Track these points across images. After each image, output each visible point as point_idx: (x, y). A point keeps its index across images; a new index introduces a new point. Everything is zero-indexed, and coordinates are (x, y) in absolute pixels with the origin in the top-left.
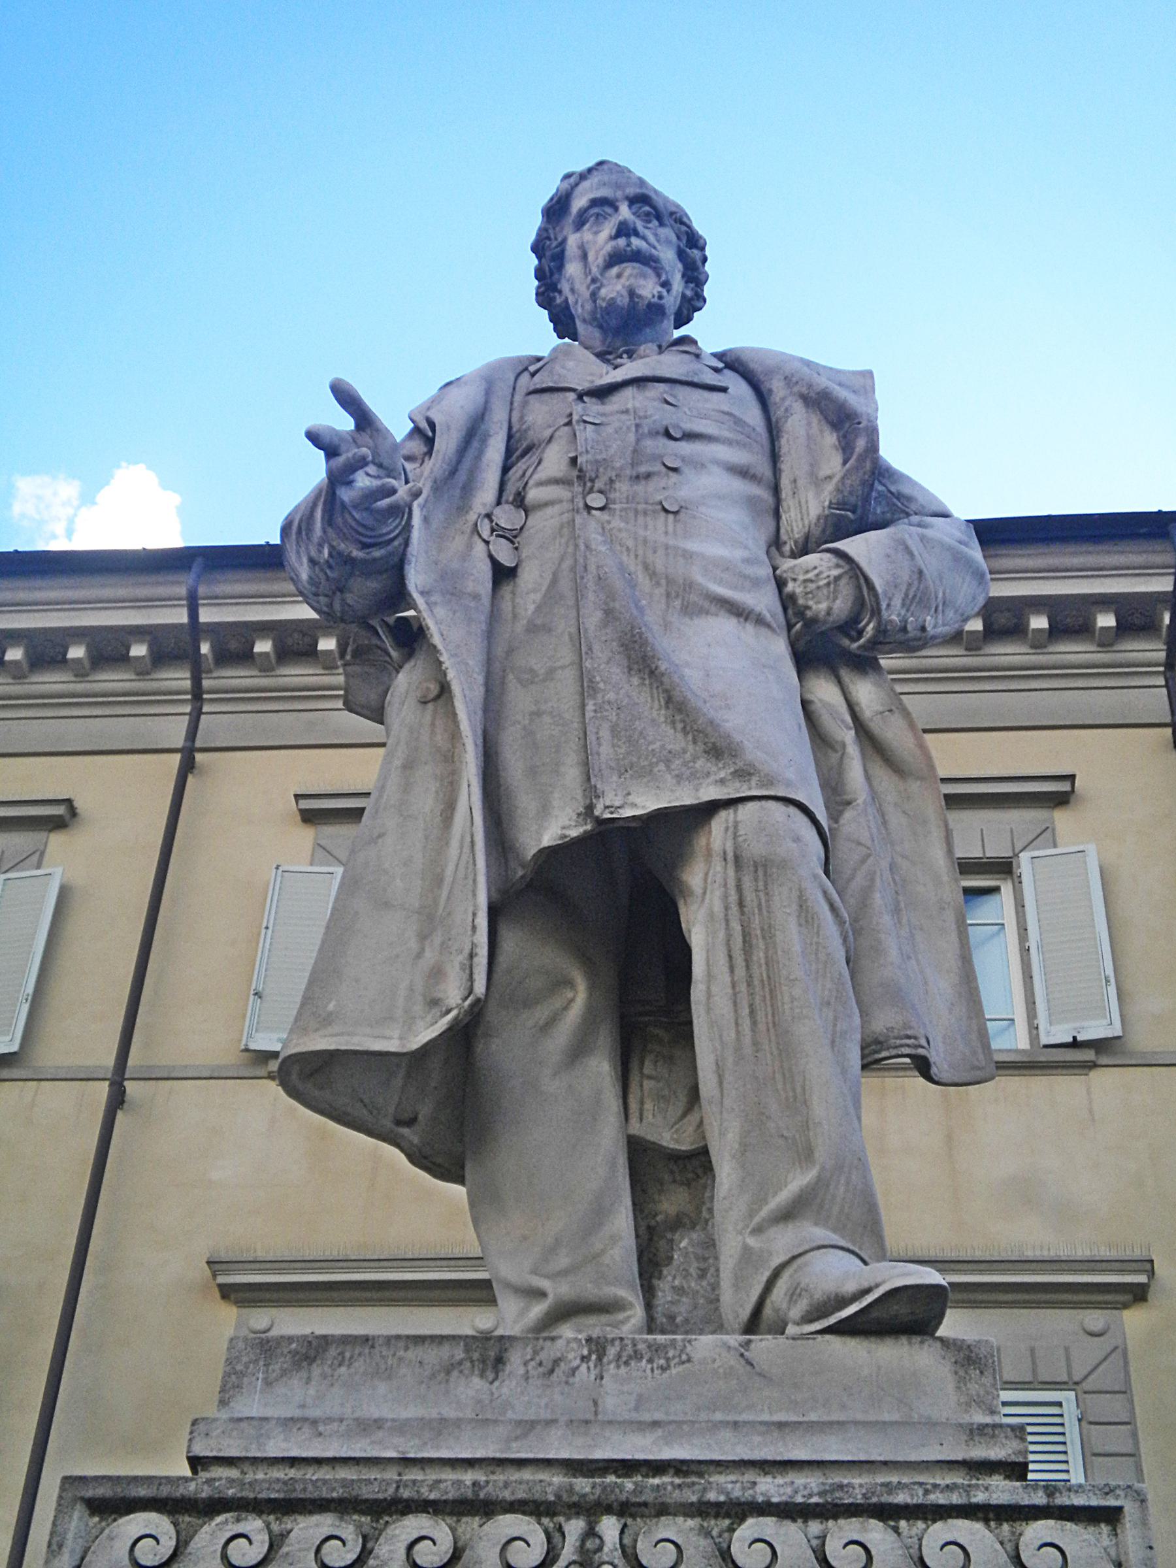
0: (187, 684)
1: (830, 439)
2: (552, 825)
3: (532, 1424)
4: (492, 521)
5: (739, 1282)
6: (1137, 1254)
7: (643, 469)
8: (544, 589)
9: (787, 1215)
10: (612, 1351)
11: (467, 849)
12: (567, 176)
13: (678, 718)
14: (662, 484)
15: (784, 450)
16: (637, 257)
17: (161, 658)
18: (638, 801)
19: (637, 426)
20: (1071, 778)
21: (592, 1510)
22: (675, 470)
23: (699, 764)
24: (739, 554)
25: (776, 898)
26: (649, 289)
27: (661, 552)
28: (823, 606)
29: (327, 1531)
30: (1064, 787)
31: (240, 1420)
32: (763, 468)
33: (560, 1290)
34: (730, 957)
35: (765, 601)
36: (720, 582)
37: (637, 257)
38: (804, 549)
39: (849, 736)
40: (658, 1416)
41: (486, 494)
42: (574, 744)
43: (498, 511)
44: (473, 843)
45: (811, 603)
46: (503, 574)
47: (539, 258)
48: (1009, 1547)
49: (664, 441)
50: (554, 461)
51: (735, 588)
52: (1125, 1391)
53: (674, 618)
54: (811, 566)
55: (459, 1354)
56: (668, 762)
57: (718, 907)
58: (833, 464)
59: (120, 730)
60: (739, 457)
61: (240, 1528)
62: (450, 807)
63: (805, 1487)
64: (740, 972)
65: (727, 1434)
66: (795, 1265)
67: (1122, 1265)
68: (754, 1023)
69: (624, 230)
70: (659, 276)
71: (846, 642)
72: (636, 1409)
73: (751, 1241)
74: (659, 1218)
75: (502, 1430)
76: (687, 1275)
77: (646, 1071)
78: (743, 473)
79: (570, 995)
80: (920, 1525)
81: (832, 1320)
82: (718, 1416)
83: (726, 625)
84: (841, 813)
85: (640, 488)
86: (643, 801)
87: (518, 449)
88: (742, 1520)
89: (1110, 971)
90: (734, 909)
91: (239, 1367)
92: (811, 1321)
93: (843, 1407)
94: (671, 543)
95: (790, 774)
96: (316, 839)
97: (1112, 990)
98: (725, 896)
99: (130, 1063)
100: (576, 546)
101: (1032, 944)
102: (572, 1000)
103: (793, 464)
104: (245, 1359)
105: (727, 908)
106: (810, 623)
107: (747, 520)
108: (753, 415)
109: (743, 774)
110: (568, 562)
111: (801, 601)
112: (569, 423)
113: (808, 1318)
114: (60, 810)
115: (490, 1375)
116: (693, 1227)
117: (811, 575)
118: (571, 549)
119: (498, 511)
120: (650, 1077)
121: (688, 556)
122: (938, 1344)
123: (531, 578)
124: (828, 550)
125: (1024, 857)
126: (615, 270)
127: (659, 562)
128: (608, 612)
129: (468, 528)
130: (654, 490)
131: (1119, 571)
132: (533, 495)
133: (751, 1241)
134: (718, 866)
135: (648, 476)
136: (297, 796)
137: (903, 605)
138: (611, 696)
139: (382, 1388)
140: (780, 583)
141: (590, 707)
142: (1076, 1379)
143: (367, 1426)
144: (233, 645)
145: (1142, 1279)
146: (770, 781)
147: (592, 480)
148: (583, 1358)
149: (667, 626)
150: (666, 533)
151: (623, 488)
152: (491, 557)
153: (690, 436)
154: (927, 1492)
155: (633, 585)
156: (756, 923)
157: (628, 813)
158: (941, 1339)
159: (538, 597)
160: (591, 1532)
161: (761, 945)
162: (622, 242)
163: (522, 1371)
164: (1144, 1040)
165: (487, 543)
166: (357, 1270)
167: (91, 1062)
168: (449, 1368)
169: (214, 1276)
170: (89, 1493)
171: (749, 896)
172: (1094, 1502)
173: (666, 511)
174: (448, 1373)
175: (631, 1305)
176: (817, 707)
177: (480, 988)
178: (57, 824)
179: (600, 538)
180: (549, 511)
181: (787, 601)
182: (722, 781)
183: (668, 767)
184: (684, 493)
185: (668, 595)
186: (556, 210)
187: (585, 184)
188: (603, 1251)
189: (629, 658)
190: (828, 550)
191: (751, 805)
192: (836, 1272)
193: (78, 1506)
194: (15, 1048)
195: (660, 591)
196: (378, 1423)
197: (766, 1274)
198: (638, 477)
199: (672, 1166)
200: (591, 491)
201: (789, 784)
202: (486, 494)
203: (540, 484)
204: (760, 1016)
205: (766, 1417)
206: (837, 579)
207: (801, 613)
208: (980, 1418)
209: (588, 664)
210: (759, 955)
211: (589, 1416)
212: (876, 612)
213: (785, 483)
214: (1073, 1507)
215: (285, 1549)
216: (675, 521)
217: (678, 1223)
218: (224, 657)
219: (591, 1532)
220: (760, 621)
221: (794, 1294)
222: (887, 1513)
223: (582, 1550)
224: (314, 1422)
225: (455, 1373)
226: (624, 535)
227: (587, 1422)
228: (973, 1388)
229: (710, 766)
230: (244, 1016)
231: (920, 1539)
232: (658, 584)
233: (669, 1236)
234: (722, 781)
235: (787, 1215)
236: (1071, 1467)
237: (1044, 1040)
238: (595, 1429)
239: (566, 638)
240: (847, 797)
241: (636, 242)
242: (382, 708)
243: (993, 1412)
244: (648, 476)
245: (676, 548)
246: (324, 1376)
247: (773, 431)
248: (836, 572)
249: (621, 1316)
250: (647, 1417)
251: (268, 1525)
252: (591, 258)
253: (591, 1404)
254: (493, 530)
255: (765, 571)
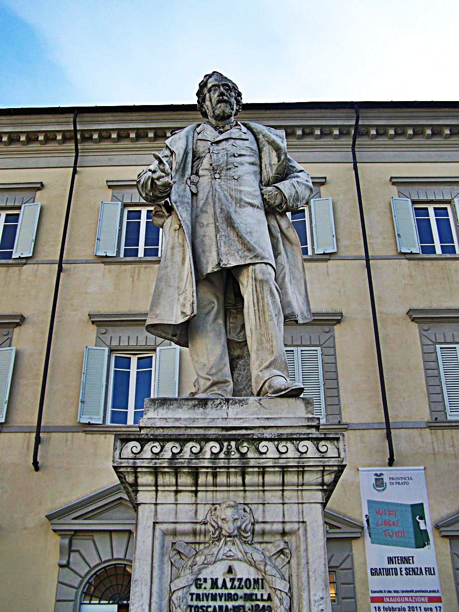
0: (74, 147)
1: (274, 154)
2: (210, 267)
3: (214, 419)
4: (190, 180)
5: (257, 383)
6: (339, 311)
7: (229, 167)
8: (204, 199)
9: (267, 368)
10: (231, 401)
11: (190, 274)
12: (206, 76)
13: (240, 240)
14: (233, 171)
15: (263, 157)
16: (225, 101)
17: (65, 140)
18: (231, 263)
19: (227, 154)
20: (325, 178)
21: (229, 440)
22: (237, 167)
23: (246, 253)
24: (253, 189)
25: (265, 290)
26: (228, 111)
27: (234, 191)
28: (273, 202)
29: (173, 445)
30: (324, 180)
31: (149, 418)
32: (258, 162)
33: (215, 379)
34: (254, 303)
35: (258, 201)
36: (248, 198)
37: (225, 101)
38: (268, 185)
39: (279, 235)
40: (241, 417)
41: (189, 172)
42: (214, 243)
43: (192, 177)
44: (191, 273)
45: (270, 201)
46: (194, 195)
47: (199, 97)
48: (316, 446)
49: (233, 158)
50: (206, 163)
51: (252, 199)
52: (334, 347)
53: (238, 209)
54: (270, 190)
55: (197, 403)
56: (238, 252)
57: (251, 290)
58: (275, 160)
59: (54, 161)
60: (252, 160)
61: (154, 445)
62: (184, 259)
63: (273, 433)
64: (256, 308)
65: (256, 420)
66: (270, 380)
67: (335, 314)
68: (260, 321)
69: (222, 94)
70: (231, 107)
71: (278, 210)
72: (237, 415)
73: (259, 373)
74: (234, 356)
75: (207, 420)
76: (240, 370)
77: (231, 321)
78: (252, 164)
79: (213, 305)
80: (298, 442)
81: (279, 394)
82: (254, 416)
83: (249, 209)
84: (277, 257)
85: (228, 172)
86: (233, 264)
87: (197, 157)
88: (261, 442)
89: (334, 234)
90: (255, 292)
91: (148, 406)
92: (274, 394)
93: (281, 414)
94: (236, 188)
95: (267, 256)
96: (113, 193)
97: (335, 239)
98: (253, 289)
99: (64, 259)
100: (213, 189)
101: (313, 225)
102: (214, 307)
103: (265, 160)
104: (149, 404)
105: (253, 291)
106: (269, 206)
107: (254, 179)
108: (255, 147)
109: (256, 257)
110: (211, 193)
111: (268, 200)
112: (209, 152)
113: (273, 393)
114: (39, 185)
115: (204, 407)
116: (242, 358)
117: (270, 193)
118: (211, 190)
119: (192, 177)
120: (231, 323)
121: (241, 191)
122: (301, 399)
123: (200, 195)
124: (274, 186)
125: (312, 200)
126: (219, 105)
127: (233, 193)
128: (222, 209)
129: (185, 182)
130: (231, 173)
131: (340, 118)
132: (201, 173)
133: (259, 373)
134: (250, 280)
135: (230, 169)
136: (107, 181)
137: (293, 201)
138: (223, 233)
139: (180, 410)
140: (262, 195)
141: (218, 236)
142: (321, 344)
143: (177, 420)
144: (87, 136)
145: (340, 318)
146: (263, 258)
147: (216, 170)
148: (224, 404)
149: (236, 212)
150: (235, 185)
151: (224, 172)
152: (191, 190)
153: (240, 155)
154: (300, 435)
155: (227, 200)
156: (260, 295)
157: (229, 266)
158: (301, 398)
159: (203, 201)
160: (229, 445)
161: (261, 301)
162: (221, 98)
163: (211, 406)
164: (343, 253)
165: (190, 187)
166: (129, 317)
167: (53, 259)
168: (195, 406)
169: (90, 318)
170: (121, 437)
171: (258, 289)
172: (334, 436)
173: (235, 179)
174: (195, 407)
175: (230, 382)
176: (271, 226)
177: (195, 312)
178: (38, 189)
179: (219, 187)
180: (205, 178)
181: (264, 200)
182: (251, 258)
183: (238, 254)
184: (239, 173)
185: (236, 203)
186: (203, 85)
187: (211, 80)
188: (223, 368)
189: (227, 223)
190: (274, 186)
191: (259, 265)
192: (280, 382)
193: (119, 440)
194: (31, 255)
195: (234, 202)
196: (180, 419)
197: (263, 381)
198: (227, 169)
199: (237, 344)
200: (216, 173)
201: (267, 259)
202: (189, 172)
203: (202, 170)
204: (261, 319)
205: (264, 417)
206: (277, 194)
207: (268, 204)
208: (311, 416)
209: (217, 224)
210: (261, 304)
211: (226, 417)
212: (286, 203)
213: (263, 165)
214: (329, 438)
215: (164, 449)
216: (237, 181)
217: (239, 357)
218: (84, 139)
219: (229, 445)
220: (258, 207)
221: (270, 387)
222: (291, 440)
223: (227, 449)
224: (166, 419)
225: (196, 407)
226: (224, 186)
227: (226, 418)
228: (309, 409)
229: (248, 254)
230: (95, 245)
231: (298, 445)
232: (233, 200)
233: (236, 360)
234: (251, 258)
235: (267, 368)
236: (319, 369)
237: (316, 253)
238: (228, 420)
239: (211, 215)
240: (280, 252)
241: (225, 98)
242: (163, 226)
243: (313, 414)
244: (230, 169)
245: (237, 190)
246: (167, 408)
247: (260, 151)
248: (276, 193)
249: (228, 384)
250: (239, 417)
251: (160, 444)
252: (213, 101)
253: (226, 414)
254: (191, 183)
255: (258, 193)
